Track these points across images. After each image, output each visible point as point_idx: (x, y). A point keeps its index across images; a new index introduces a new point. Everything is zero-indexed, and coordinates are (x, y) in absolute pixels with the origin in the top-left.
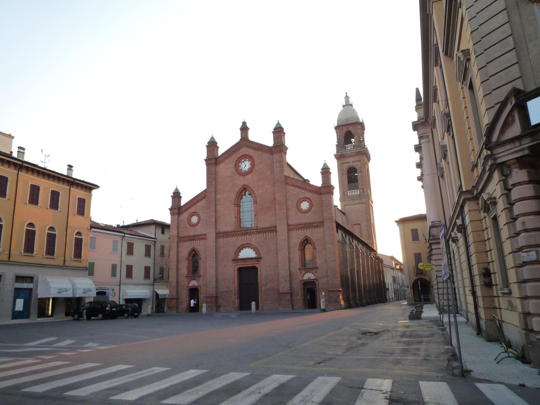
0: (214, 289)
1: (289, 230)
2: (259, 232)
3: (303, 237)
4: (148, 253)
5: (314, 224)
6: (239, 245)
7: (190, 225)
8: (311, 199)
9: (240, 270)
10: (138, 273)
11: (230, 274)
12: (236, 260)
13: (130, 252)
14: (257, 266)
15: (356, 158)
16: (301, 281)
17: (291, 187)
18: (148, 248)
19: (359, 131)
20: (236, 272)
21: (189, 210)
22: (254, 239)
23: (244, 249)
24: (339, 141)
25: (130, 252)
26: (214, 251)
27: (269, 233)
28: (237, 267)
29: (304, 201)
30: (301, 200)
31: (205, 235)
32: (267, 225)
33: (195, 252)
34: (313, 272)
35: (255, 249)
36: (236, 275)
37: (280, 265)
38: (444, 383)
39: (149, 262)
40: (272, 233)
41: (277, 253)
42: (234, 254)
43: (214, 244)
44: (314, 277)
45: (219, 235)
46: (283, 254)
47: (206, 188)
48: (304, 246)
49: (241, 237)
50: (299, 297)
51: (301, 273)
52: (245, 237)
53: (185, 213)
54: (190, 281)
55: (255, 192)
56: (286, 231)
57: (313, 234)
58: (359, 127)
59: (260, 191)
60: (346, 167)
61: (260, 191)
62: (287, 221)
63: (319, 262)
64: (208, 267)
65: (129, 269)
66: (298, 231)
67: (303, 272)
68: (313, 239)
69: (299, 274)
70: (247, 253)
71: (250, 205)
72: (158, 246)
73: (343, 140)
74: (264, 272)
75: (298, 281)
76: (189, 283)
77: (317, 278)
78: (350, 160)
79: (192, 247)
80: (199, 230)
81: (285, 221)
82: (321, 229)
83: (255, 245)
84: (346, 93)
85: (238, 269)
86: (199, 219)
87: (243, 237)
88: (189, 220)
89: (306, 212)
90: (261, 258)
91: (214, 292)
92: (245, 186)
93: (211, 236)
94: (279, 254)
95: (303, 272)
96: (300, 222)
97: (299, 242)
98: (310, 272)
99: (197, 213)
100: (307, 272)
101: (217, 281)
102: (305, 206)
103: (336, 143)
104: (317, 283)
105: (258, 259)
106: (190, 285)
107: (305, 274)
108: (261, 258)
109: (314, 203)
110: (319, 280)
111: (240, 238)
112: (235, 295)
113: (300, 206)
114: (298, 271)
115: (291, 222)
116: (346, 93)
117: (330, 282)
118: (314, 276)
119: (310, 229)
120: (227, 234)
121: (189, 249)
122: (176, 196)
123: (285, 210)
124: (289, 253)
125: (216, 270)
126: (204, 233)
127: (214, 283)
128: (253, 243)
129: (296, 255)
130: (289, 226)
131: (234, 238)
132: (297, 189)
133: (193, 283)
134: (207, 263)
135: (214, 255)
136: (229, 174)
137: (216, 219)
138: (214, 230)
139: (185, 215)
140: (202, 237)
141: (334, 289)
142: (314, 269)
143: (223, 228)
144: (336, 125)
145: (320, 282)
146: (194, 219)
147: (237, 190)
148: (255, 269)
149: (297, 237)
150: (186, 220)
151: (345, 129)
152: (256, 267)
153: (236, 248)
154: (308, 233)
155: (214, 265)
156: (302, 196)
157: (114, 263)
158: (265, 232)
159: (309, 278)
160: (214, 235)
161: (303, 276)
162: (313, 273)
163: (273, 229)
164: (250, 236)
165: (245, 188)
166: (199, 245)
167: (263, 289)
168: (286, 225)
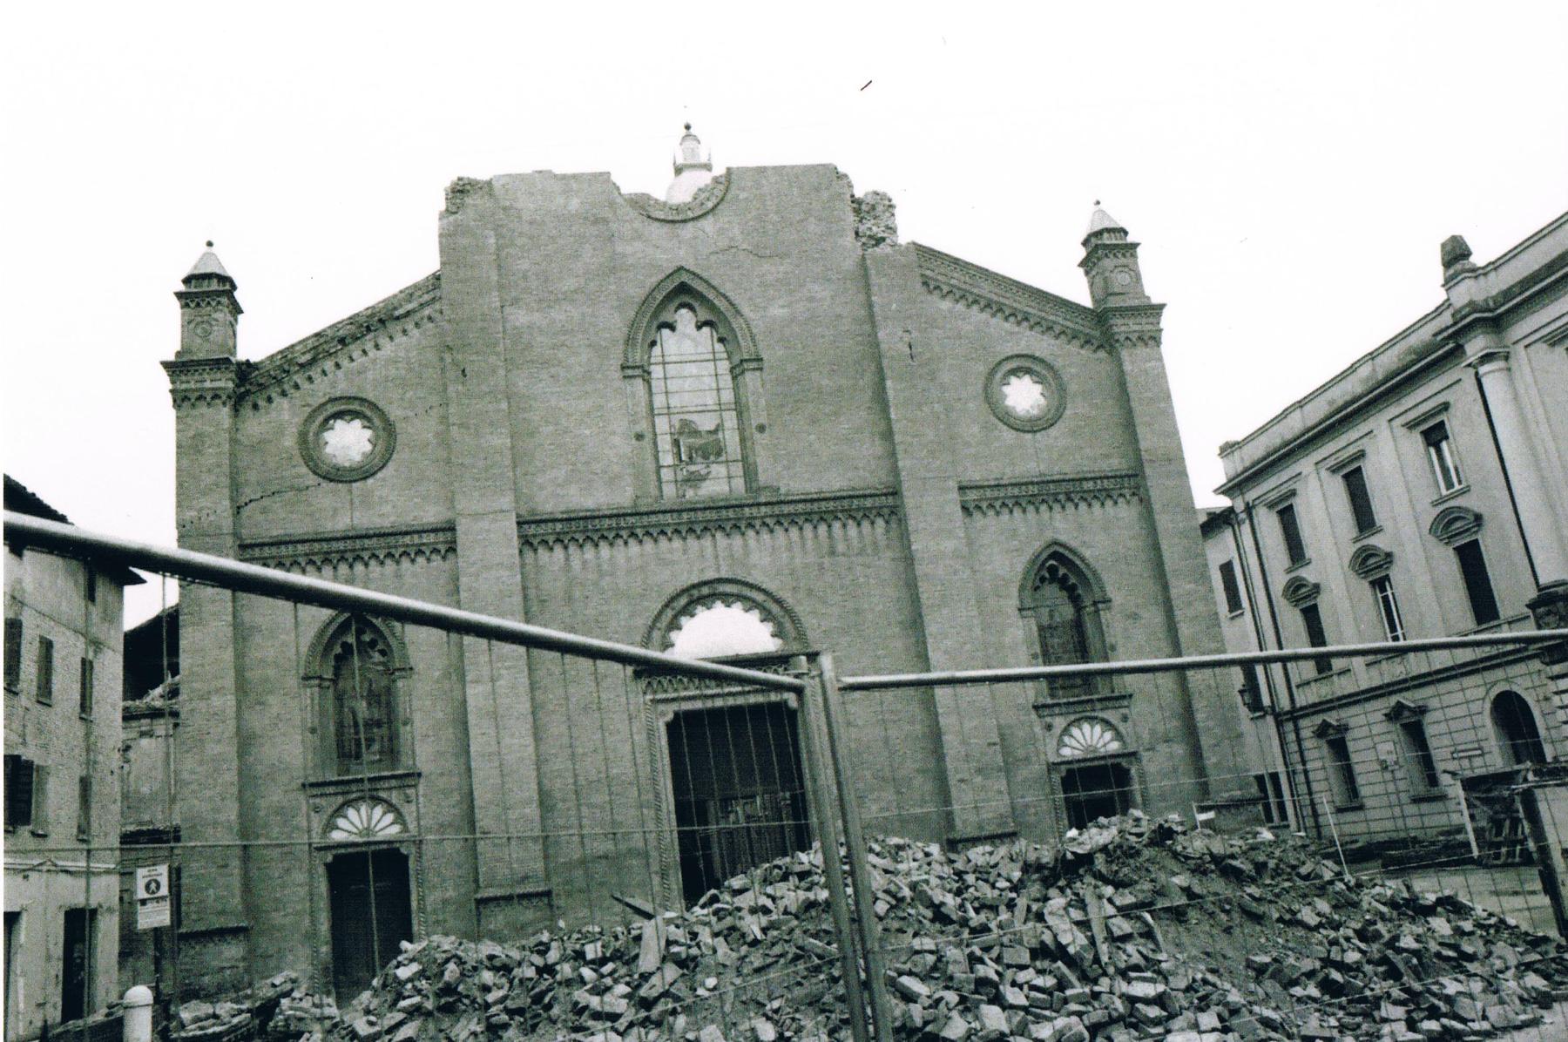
5: (1089, 485)
6: (670, 590)
8: (1059, 363)
16: (1052, 767)
17: (946, 305)
22: (761, 555)
23: (702, 614)
28: (669, 712)
44: (1114, 746)
47: (424, 261)
51: (1049, 727)
54: (339, 812)
59: (777, 311)
66: (1005, 517)
69: (1038, 729)
70: (720, 634)
71: (710, 382)
75: (1038, 768)
76: (330, 826)
84: (688, 127)
87: (692, 541)
90: (419, 775)
92: (685, 278)
95: (1059, 723)
96: (1010, 473)
100: (1077, 722)
101: (545, 801)
108: (419, 775)
109: (1073, 387)
110: (1146, 756)
111: (672, 547)
112: (664, 875)
114: (1034, 716)
116: (688, 127)
118: (1119, 736)
122: (208, 293)
128: (756, 577)
131: (634, 547)
132: (977, 315)
133: (364, 823)
136: (575, 204)
139: (281, 417)
146: (348, 441)
147: (638, 293)
149: (1009, 546)
150: (290, 442)
162: (391, 807)
164: (737, 540)
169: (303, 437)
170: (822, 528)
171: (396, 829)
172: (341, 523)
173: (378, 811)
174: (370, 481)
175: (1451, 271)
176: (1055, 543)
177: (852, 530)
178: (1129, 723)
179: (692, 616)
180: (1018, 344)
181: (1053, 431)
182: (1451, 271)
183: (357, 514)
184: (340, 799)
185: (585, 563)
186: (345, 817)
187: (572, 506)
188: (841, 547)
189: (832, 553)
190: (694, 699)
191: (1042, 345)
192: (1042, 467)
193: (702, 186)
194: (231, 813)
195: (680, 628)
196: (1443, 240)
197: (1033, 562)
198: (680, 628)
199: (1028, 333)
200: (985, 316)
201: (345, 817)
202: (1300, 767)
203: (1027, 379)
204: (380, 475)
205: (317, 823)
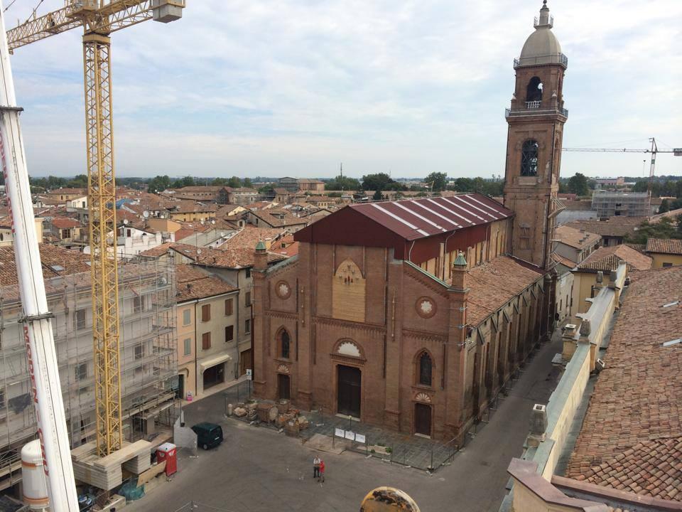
3: (420, 348)
4: (228, 312)
6: (339, 338)
10: (218, 338)
13: (206, 317)
15: (541, 126)
16: (413, 401)
17: (410, 278)
18: (228, 303)
24: (517, 93)
25: (206, 317)
29: (427, 301)
30: (423, 299)
33: (285, 330)
35: (359, 347)
36: (334, 373)
39: (230, 321)
50: (409, 418)
51: (414, 392)
60: (521, 138)
65: (206, 337)
66: (414, 339)
67: (416, 392)
68: (433, 353)
70: (349, 349)
72: (242, 296)
73: (524, 93)
76: (278, 368)
78: (530, 128)
83: (360, 343)
87: (345, 328)
89: (426, 316)
90: (366, 361)
95: (416, 392)
97: (414, 354)
98: (425, 394)
99: (286, 282)
102: (426, 307)
104: (432, 408)
105: (361, 361)
107: (418, 394)
118: (430, 399)
132: (418, 284)
145: (436, 409)
148: (358, 371)
149: (412, 347)
151: (531, 74)
152: (359, 369)
158: (373, 329)
162: (428, 396)
169: (275, 287)
170: (372, 332)
172: (281, 308)
175: (14, 481)
176: (425, 348)
181: (432, 319)
182: (14, 481)
189: (373, 338)
190: (341, 362)
191: (434, 295)
193: (564, 77)
194: (261, 362)
197: (418, 351)
202: (10, 462)
205: (276, 367)
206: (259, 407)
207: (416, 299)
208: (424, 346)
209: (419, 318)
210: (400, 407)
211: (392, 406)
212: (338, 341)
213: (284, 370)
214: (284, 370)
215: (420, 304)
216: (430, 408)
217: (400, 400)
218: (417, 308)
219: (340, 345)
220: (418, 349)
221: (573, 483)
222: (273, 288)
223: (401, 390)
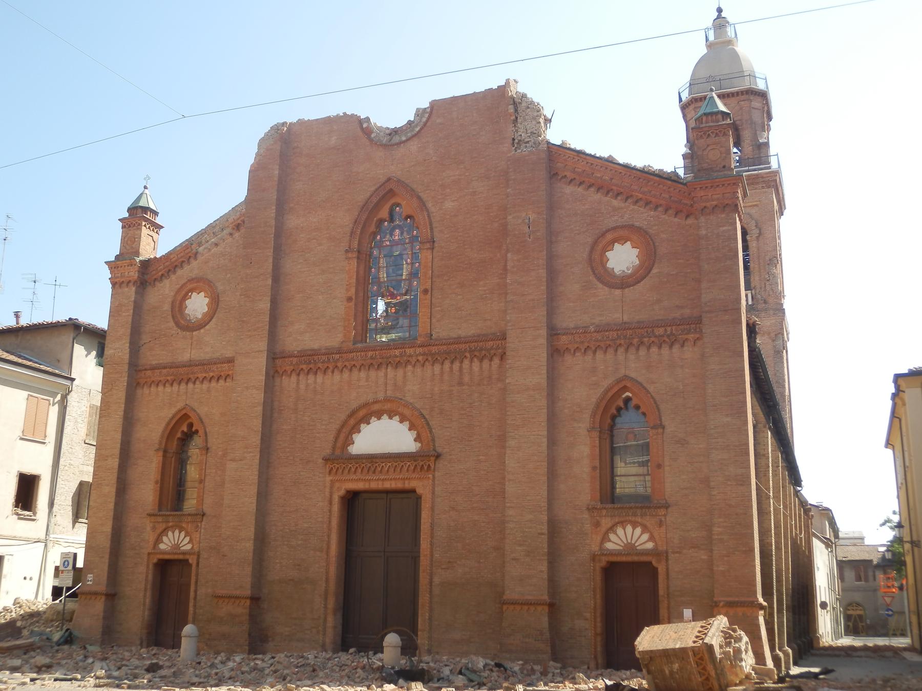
0: (248, 570)
1: (555, 352)
2: (434, 359)
6: (354, 405)
7: (177, 324)
9: (352, 500)
11: (312, 510)
12: (339, 459)
14: (421, 486)
16: (594, 558)
19: (756, 116)
20: (336, 508)
21: (179, 272)
22: (414, 382)
26: (257, 424)
27: (476, 363)
29: (622, 240)
30: (609, 236)
31: (231, 361)
32: (467, 330)
34: (649, 521)
35: (418, 423)
36: (335, 522)
37: (510, 488)
38: (643, 633)
40: (486, 363)
41: (502, 439)
42: (331, 437)
43: (259, 396)
44: (650, 545)
45: (278, 362)
46: (527, 446)
48: (614, 418)
49: (363, 374)
51: (597, 524)
52: (381, 373)
53: (166, 282)
54: (164, 532)
55: (429, 205)
56: (543, 355)
57: (656, 372)
58: (757, 103)
59: (449, 205)
61: (449, 205)
62: (551, 313)
63: (673, 483)
64: (226, 480)
69: (588, 527)
70: (385, 436)
74: (443, 509)
76: (158, 540)
77: (663, 548)
79: (180, 405)
80: (211, 345)
81: (541, 313)
82: (689, 353)
85: (343, 498)
86: (215, 302)
87: (373, 373)
88: (178, 306)
89: (625, 282)
90: (438, 456)
91: (247, 581)
93: (253, 366)
94: (511, 443)
95: (606, 523)
98: (635, 525)
101: (261, 539)
103: (684, 150)
104: (661, 569)
105: (425, 459)
106: (162, 546)
107: (612, 529)
110: (672, 556)
113: (603, 261)
114: (586, 515)
115: (571, 317)
117: (720, 567)
119: (643, 352)
120: (313, 362)
121: (168, 413)
122: (138, 217)
123: (543, 273)
124: (552, 442)
125: (263, 495)
126: (229, 354)
127: (249, 545)
129: (582, 450)
130: (553, 333)
131: (337, 376)
132: (595, 196)
134: (231, 466)
135: (256, 440)
136: (334, 140)
137: (274, 302)
138: (263, 345)
139: (165, 290)
140: (218, 370)
141: (743, 599)
142: (643, 506)
143: (300, 336)
144: (685, 96)
149: (583, 386)
150: (167, 307)
153: (343, 417)
154: (633, 365)
155: (252, 475)
156: (611, 222)
157: (29, 470)
158: (458, 357)
159: (630, 547)
160: (261, 362)
161: (605, 538)
162: (645, 529)
163: (490, 347)
165: (391, 193)
166: (205, 401)
167: (436, 580)
168: (544, 332)
170: (456, 365)
171: (189, 547)
173: (638, 530)
174: (202, 331)
176: (626, 377)
177: (476, 364)
178: (663, 529)
179: (369, 423)
180: (622, 217)
181: (639, 287)
183: (193, 352)
184: (164, 526)
185: (307, 385)
186: (610, 541)
187: (306, 347)
188: (466, 379)
189: (460, 383)
191: (642, 217)
192: (626, 319)
195: (410, 430)
196: (291, 115)
198: (410, 430)
199: (632, 207)
200: (598, 196)
201: (610, 541)
203: (617, 246)
204: (207, 327)
206: (201, 446)
207: (590, 240)
208: (622, 372)
209: (602, 291)
210: (553, 582)
211: (526, 578)
212: (350, 416)
213: (177, 546)
214: (177, 546)
215: (606, 269)
216: (655, 571)
217: (553, 557)
218: (596, 264)
219: (356, 429)
220: (606, 384)
221: (776, 207)
222: (185, 273)
223: (554, 528)
